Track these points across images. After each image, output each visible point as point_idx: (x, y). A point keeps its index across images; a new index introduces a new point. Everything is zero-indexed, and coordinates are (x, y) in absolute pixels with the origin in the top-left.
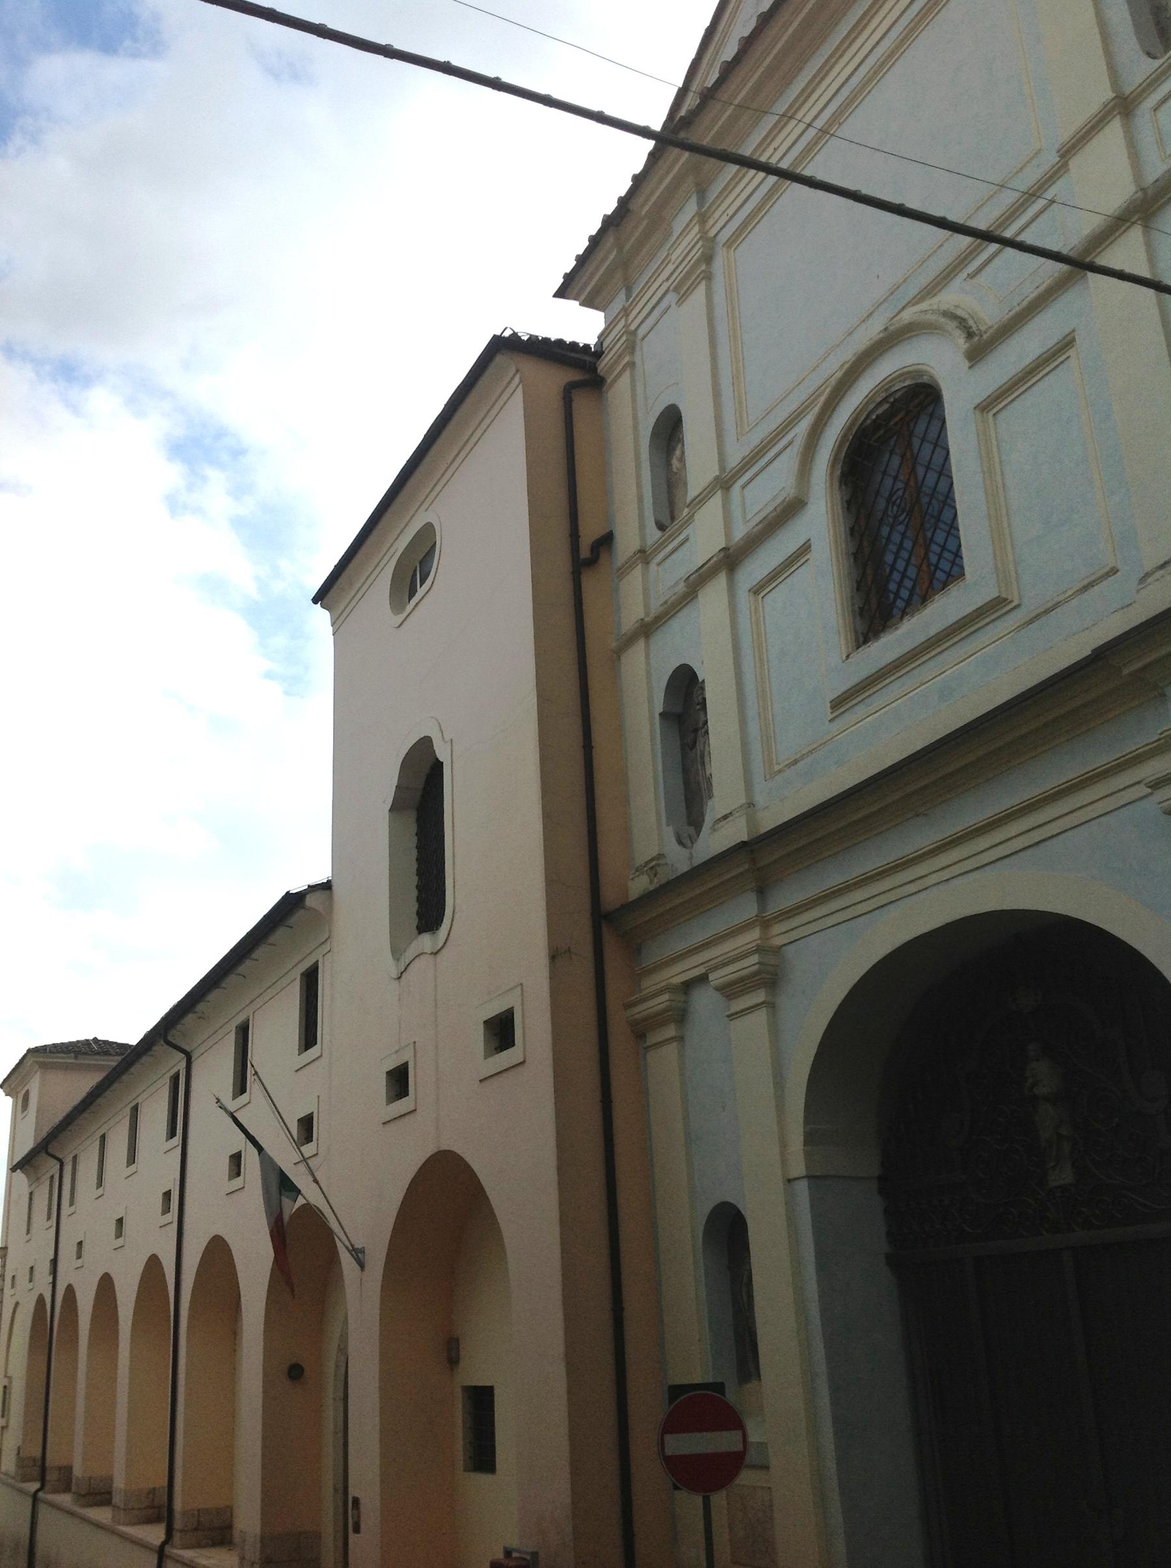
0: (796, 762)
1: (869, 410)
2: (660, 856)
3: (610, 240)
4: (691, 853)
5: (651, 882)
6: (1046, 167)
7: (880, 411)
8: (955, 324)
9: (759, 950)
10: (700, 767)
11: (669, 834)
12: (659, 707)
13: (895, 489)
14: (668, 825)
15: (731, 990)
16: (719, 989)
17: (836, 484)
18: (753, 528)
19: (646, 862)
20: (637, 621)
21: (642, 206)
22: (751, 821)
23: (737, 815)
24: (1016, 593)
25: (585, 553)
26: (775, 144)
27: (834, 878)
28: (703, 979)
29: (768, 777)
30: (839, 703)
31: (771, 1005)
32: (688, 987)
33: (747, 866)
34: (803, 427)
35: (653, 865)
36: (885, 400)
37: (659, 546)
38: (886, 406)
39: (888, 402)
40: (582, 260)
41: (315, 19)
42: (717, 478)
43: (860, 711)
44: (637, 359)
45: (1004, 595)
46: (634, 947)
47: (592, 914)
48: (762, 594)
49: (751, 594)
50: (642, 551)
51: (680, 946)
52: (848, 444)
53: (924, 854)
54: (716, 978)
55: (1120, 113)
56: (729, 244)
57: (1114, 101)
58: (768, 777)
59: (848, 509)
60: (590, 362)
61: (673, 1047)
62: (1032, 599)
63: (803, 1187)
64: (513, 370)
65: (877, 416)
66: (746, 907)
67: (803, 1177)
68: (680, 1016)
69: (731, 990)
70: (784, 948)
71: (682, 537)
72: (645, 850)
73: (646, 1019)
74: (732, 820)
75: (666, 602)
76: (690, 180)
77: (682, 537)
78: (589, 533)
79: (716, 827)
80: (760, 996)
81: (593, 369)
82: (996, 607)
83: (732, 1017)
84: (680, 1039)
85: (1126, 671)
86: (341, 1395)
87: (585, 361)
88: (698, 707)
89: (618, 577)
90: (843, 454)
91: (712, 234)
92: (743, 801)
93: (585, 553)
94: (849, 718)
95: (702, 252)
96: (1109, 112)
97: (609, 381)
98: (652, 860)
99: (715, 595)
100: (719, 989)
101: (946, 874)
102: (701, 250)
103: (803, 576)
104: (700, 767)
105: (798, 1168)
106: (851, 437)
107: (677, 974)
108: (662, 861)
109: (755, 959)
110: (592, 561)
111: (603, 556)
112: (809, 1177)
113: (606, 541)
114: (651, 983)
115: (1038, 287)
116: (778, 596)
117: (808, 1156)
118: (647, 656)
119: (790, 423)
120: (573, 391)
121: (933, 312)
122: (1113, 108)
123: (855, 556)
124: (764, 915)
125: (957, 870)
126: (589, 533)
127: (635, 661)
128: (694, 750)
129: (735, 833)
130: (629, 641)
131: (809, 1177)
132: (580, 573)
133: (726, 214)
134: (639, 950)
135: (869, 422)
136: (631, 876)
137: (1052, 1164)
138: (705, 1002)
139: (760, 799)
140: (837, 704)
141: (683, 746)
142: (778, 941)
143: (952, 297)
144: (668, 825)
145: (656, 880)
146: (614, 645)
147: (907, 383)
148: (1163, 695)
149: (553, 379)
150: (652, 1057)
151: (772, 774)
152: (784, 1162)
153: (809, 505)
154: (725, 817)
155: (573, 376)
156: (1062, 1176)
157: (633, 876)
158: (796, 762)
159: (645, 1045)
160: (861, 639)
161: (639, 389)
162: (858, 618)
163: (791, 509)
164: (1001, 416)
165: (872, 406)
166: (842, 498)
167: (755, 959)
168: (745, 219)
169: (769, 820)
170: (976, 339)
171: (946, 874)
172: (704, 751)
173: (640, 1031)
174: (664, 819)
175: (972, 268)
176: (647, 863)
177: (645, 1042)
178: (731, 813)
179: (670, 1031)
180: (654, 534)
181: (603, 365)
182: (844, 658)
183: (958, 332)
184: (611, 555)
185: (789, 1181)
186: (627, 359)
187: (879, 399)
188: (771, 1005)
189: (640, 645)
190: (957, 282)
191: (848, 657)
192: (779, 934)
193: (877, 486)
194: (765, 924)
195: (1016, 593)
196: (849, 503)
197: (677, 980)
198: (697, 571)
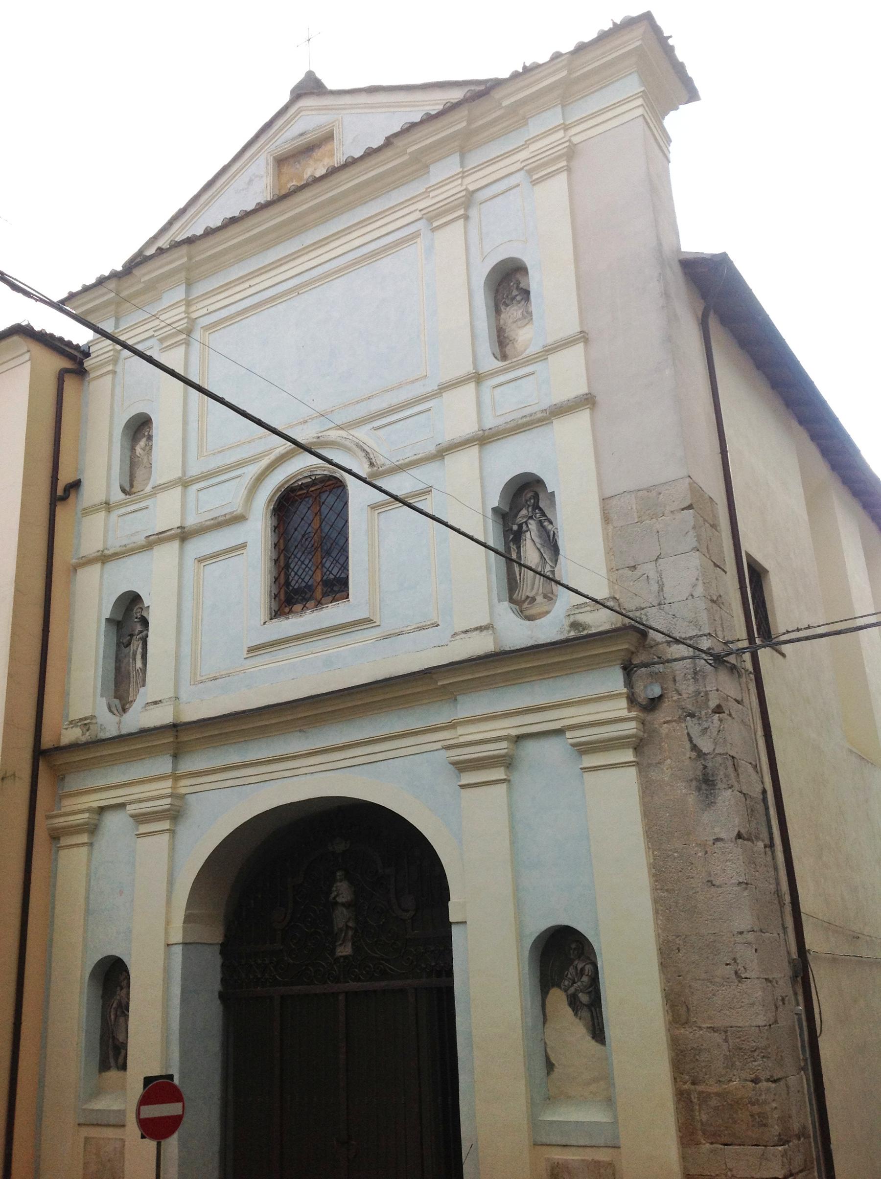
0: (215, 679)
1: (297, 478)
2: (93, 717)
3: (112, 285)
4: (120, 720)
5: (83, 734)
6: (429, 389)
7: (304, 481)
8: (363, 454)
9: (171, 796)
10: (131, 661)
11: (102, 703)
12: (107, 613)
13: (307, 532)
14: (102, 696)
15: (140, 818)
16: (132, 816)
17: (269, 515)
18: (206, 521)
19: (80, 719)
20: (98, 551)
21: (144, 275)
22: (176, 712)
23: (166, 704)
24: (378, 617)
25: (60, 492)
26: (252, 282)
27: (233, 757)
28: (122, 806)
29: (192, 683)
30: (253, 650)
31: (172, 832)
32: (102, 810)
33: (171, 739)
34: (253, 470)
35: (86, 723)
36: (310, 476)
37: (120, 505)
38: (309, 480)
39: (311, 478)
40: (86, 289)
41: (471, 534)
42: (180, 478)
43: (267, 658)
44: (119, 369)
45: (372, 618)
46: (59, 777)
47: (34, 751)
48: (204, 564)
49: (196, 561)
50: (107, 503)
51: (102, 783)
52: (280, 493)
53: (301, 755)
54: (132, 809)
55: (475, 381)
56: (206, 328)
57: (473, 375)
58: (192, 683)
59: (274, 531)
60: (80, 358)
61: (84, 850)
62: (389, 624)
63: (178, 951)
64: (26, 349)
65: (302, 483)
66: (163, 765)
67: (179, 944)
68: (92, 829)
69: (140, 818)
70: (187, 795)
71: (142, 505)
72: (78, 710)
73: (64, 828)
74: (162, 707)
75: (125, 546)
76: (183, 275)
77: (142, 505)
78: (65, 478)
79: (147, 708)
80: (166, 825)
81: (81, 363)
82: (366, 622)
83: (139, 836)
84: (91, 845)
85: (440, 683)
86: (99, 1122)
87: (76, 356)
88: (136, 620)
89: (82, 514)
90: (276, 498)
91: (194, 316)
92: (172, 694)
93: (60, 492)
94: (259, 660)
95: (186, 327)
96: (469, 379)
97: (92, 375)
98: (86, 719)
99: (168, 552)
100: (132, 816)
101: (312, 769)
102: (186, 325)
103: (235, 562)
104: (131, 661)
105: (177, 936)
106: (283, 490)
107: (95, 801)
108: (94, 721)
109: (169, 801)
110: (64, 498)
111: (72, 496)
112: (185, 944)
113: (76, 485)
114: (69, 804)
115: (415, 455)
116: (215, 569)
117: (185, 930)
118: (101, 577)
119: (240, 464)
120: (65, 375)
121: (352, 441)
122: (472, 378)
123: (276, 561)
124: (176, 772)
125: (322, 768)
126: (65, 478)
127: (89, 577)
128: (127, 648)
129: (162, 716)
130: (88, 562)
131: (185, 944)
132: (55, 506)
133: (206, 308)
134: (63, 779)
135: (296, 484)
136: (65, 727)
137: (340, 942)
138: (114, 822)
139: (184, 696)
140: (251, 650)
141: (119, 644)
142: (183, 791)
143: (362, 434)
144: (102, 696)
145: (88, 733)
146: (74, 561)
147: (325, 473)
148: (456, 700)
149: (55, 363)
150: (62, 853)
151: (195, 682)
152: (167, 933)
153: (248, 521)
154: (155, 703)
155: (66, 364)
156: (345, 950)
157: (67, 726)
158: (215, 679)
159: (58, 845)
160: (273, 614)
161: (118, 390)
162: (273, 600)
163: (237, 519)
164: (382, 516)
165: (300, 477)
166: (271, 524)
167: (169, 801)
168: (221, 319)
169: (191, 714)
170: (376, 468)
171: (312, 769)
172: (136, 652)
173: (55, 836)
174: (99, 691)
175: (377, 424)
176: (81, 720)
177: (59, 843)
178: (160, 701)
179: (84, 838)
180: (118, 496)
181: (88, 363)
182: (262, 624)
183: (365, 460)
184: (77, 497)
185: (168, 945)
186: (110, 368)
187: (306, 475)
188: (172, 832)
189: (98, 566)
190: (369, 427)
191: (265, 623)
192: (185, 785)
193: (296, 526)
194: (176, 777)
195: (378, 617)
196: (275, 528)
197: (96, 805)
198: (157, 534)
